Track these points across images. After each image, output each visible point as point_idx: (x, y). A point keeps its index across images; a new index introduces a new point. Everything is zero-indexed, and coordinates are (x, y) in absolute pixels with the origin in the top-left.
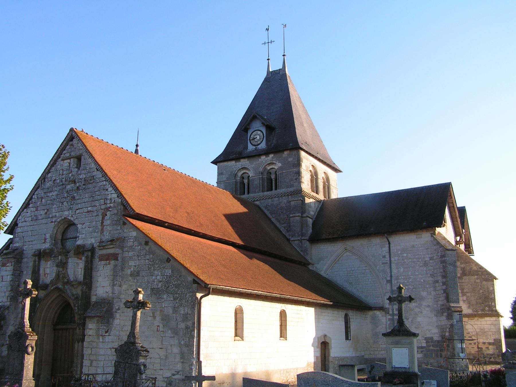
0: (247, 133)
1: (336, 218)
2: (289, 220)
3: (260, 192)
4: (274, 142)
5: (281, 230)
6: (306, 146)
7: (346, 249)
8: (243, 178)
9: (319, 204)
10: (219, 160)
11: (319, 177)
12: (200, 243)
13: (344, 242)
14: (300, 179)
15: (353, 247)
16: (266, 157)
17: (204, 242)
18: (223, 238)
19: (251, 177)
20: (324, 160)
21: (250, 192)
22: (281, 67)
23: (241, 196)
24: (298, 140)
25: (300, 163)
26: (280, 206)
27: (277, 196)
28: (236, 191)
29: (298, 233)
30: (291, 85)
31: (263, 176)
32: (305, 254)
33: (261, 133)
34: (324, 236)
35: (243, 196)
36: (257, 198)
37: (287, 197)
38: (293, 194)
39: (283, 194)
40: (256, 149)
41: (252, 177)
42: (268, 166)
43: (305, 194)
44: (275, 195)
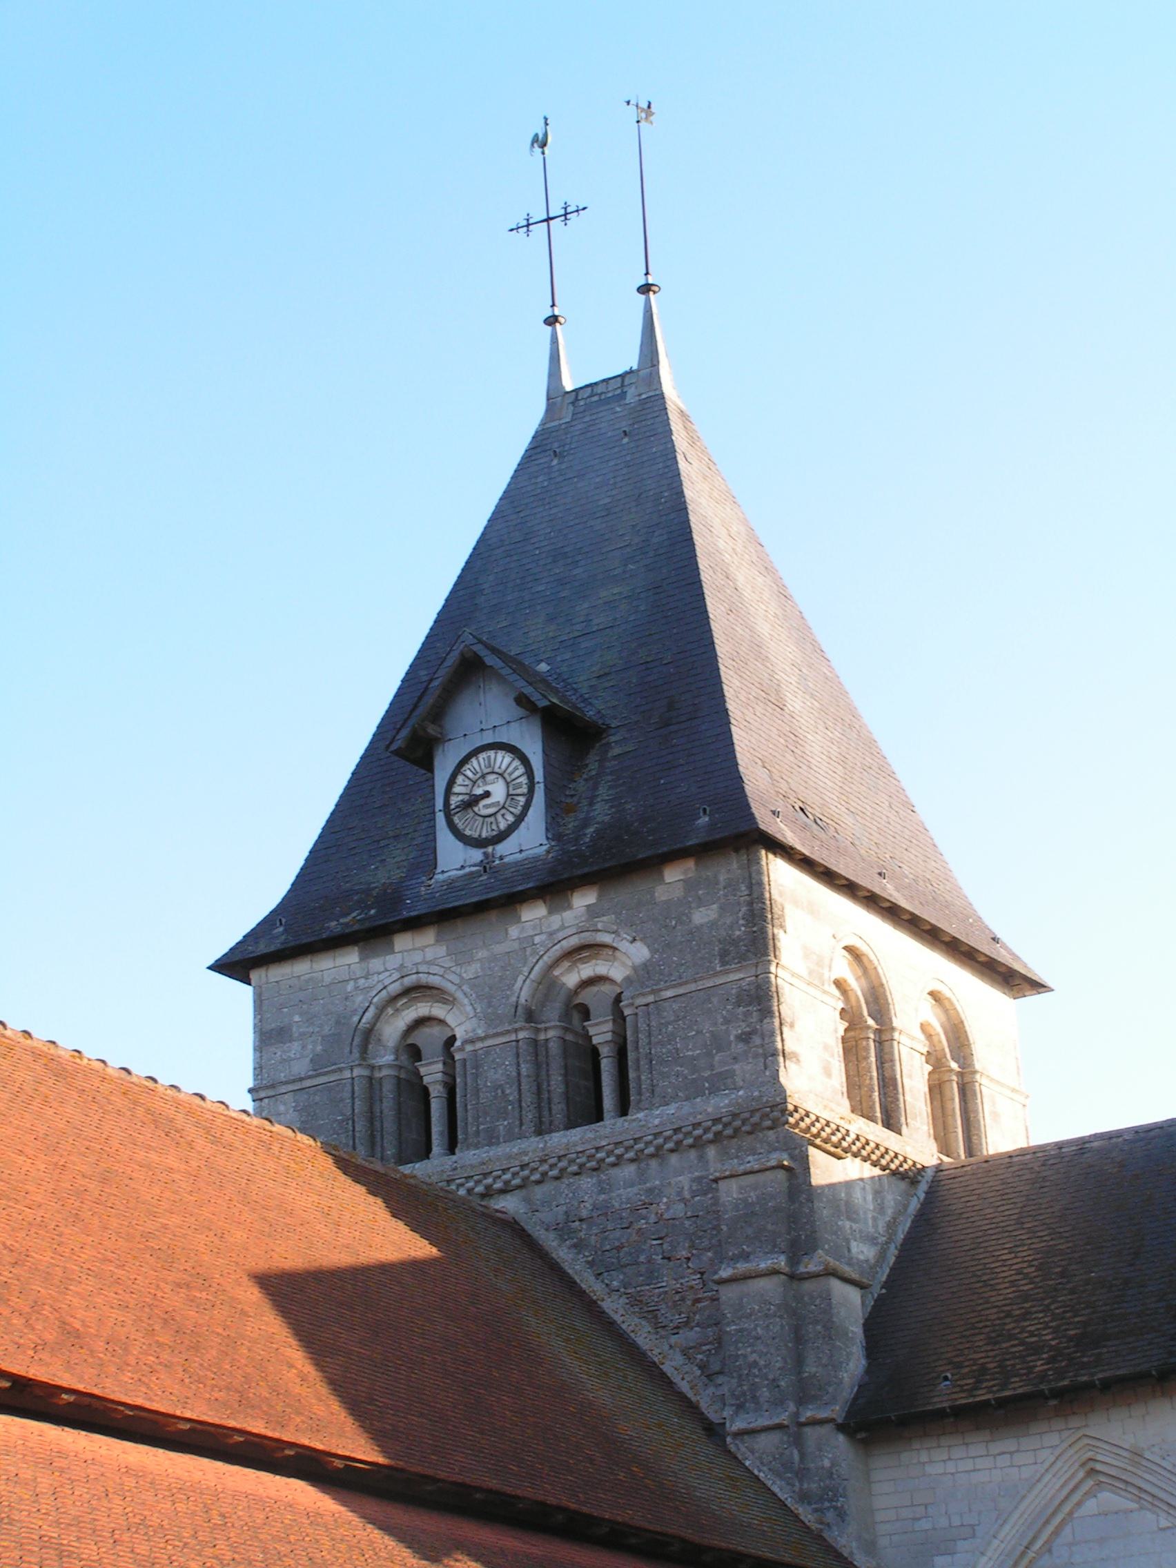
0: (429, 767)
1: (1019, 1272)
2: (714, 1300)
3: (521, 1136)
4: (601, 812)
5: (667, 1368)
6: (805, 827)
7: (1093, 1471)
8: (415, 1053)
9: (908, 1195)
10: (263, 948)
11: (896, 1023)
12: (50, 1460)
13: (1075, 1422)
14: (772, 1034)
15: (1137, 1454)
16: (550, 912)
17: (89, 1456)
18: (232, 1423)
19: (465, 1042)
20: (925, 916)
21: (460, 1137)
22: (629, 359)
23: (406, 1169)
24: (748, 789)
25: (763, 931)
26: (653, 1218)
27: (631, 1155)
28: (372, 1136)
29: (774, 1384)
30: (695, 463)
31: (538, 1030)
32: (830, 1516)
33: (517, 763)
34: (944, 1395)
35: (419, 1170)
36: (507, 1176)
37: (693, 1154)
38: (729, 1132)
39: (667, 1139)
40: (486, 866)
41: (472, 1041)
42: (566, 964)
43: (808, 1130)
44: (617, 1144)
